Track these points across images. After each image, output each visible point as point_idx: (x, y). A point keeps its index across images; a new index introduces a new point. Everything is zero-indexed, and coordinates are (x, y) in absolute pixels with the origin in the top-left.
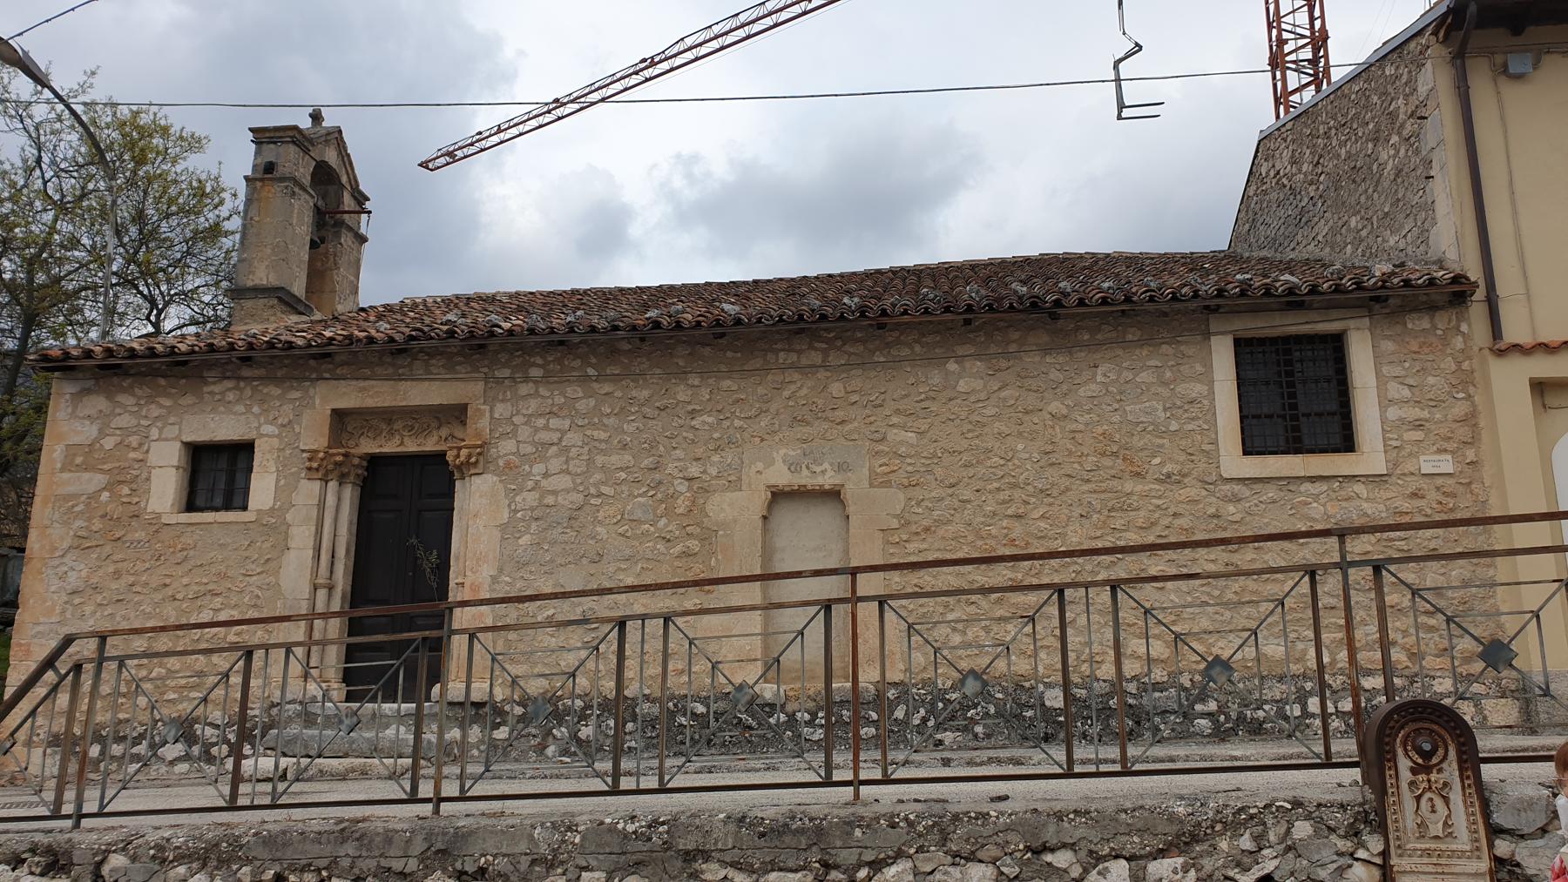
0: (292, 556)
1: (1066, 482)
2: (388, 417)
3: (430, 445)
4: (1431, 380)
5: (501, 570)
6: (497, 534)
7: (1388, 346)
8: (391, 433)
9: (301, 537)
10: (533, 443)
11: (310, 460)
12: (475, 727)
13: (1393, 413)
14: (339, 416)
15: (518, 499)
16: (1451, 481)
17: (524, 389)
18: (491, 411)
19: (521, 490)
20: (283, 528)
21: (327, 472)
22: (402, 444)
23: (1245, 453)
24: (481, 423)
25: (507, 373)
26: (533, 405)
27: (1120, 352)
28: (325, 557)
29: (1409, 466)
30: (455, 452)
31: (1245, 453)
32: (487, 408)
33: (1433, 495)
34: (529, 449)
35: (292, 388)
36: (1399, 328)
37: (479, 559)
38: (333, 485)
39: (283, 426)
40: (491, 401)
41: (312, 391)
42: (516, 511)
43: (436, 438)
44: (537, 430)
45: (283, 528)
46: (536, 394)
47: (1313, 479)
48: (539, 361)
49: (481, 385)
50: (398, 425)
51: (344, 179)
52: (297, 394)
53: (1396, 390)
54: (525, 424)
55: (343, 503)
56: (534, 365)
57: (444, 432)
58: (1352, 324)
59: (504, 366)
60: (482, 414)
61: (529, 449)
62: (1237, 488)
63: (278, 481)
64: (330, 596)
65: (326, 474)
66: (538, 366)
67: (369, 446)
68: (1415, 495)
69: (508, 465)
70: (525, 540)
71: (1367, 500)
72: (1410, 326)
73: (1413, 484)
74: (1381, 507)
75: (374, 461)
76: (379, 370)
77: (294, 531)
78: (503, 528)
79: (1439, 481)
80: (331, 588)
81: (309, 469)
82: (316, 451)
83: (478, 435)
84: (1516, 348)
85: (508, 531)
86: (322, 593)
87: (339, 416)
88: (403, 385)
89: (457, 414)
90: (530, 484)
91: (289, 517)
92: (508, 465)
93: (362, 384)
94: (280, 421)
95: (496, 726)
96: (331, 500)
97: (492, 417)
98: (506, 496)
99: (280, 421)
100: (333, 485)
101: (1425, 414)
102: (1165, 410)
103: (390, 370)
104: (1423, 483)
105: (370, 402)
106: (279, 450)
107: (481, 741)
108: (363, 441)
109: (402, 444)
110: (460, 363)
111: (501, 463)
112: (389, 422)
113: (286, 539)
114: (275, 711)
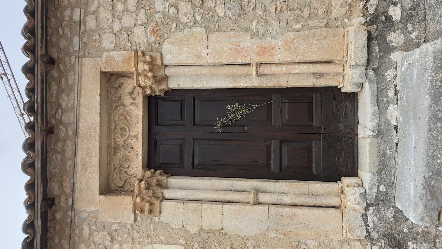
0: (230, 226)
2: (111, 150)
3: (137, 112)
5: (247, 30)
6: (214, 36)
8: (126, 146)
9: (212, 217)
10: (137, 12)
11: (142, 211)
12: (389, 38)
14: (107, 189)
15: (184, 20)
17: (91, 23)
18: (108, 51)
19: (177, 18)
20: (203, 234)
21: (154, 195)
22: (136, 137)
24: (118, 59)
25: (76, 39)
26: (105, 14)
30: (142, 78)
32: (105, 54)
34: (142, 14)
35: (80, 234)
37: (236, 51)
38: (167, 193)
39: (112, 240)
40: (100, 51)
41: (84, 215)
42: (195, 22)
43: (133, 108)
44: (126, 10)
45: (203, 234)
46: (96, 13)
48: (67, 12)
50: (120, 141)
52: (86, 229)
54: (120, 20)
55: (181, 186)
56: (71, 17)
57: (127, 100)
59: (70, 42)
60: (111, 58)
61: (142, 14)
63: (161, 243)
64: (264, 192)
65: (158, 198)
66: (72, 13)
67: (136, 165)
69: (156, 32)
70: (220, 11)
75: (152, 162)
76: (69, 152)
77: (206, 225)
78: (209, 31)
80: (257, 191)
81: (151, 212)
82: (135, 205)
83: (128, 60)
85: (212, 25)
86: (263, 198)
87: (107, 189)
88: (83, 130)
89: (111, 80)
90: (172, 10)
91: (193, 230)
92: (156, 32)
93: (79, 168)
94: (108, 243)
95: (389, 18)
97: (114, 50)
98: (182, 31)
99: (108, 243)
100: (167, 193)
103: (69, 143)
105: (96, 160)
106: (133, 242)
107: (404, 30)
108: (131, 171)
109: (136, 137)
110: (67, 80)
111: (153, 39)
112: (116, 149)
113: (213, 232)
114: (374, 235)
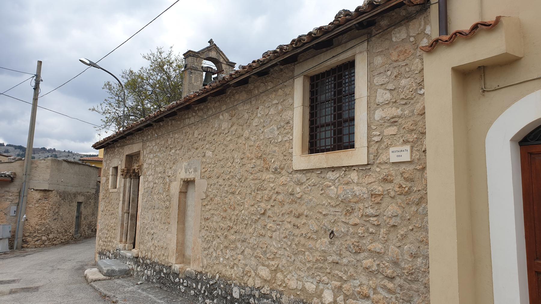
1: (246, 174)
4: (403, 82)
7: (379, 60)
13: (379, 114)
16: (411, 167)
23: (353, 147)
27: (265, 98)
28: (126, 203)
29: (383, 158)
31: (353, 147)
33: (399, 180)
36: (386, 44)
47: (333, 169)
49: (141, 144)
51: (221, 60)
53: (383, 96)
58: (357, 49)
62: (299, 176)
68: (385, 180)
71: (358, 184)
72: (394, 39)
73: (384, 171)
74: (364, 190)
79: (402, 168)
84: (459, 34)
96: (128, 185)
100: (128, 180)
101: (399, 112)
102: (278, 129)
104: (393, 171)
